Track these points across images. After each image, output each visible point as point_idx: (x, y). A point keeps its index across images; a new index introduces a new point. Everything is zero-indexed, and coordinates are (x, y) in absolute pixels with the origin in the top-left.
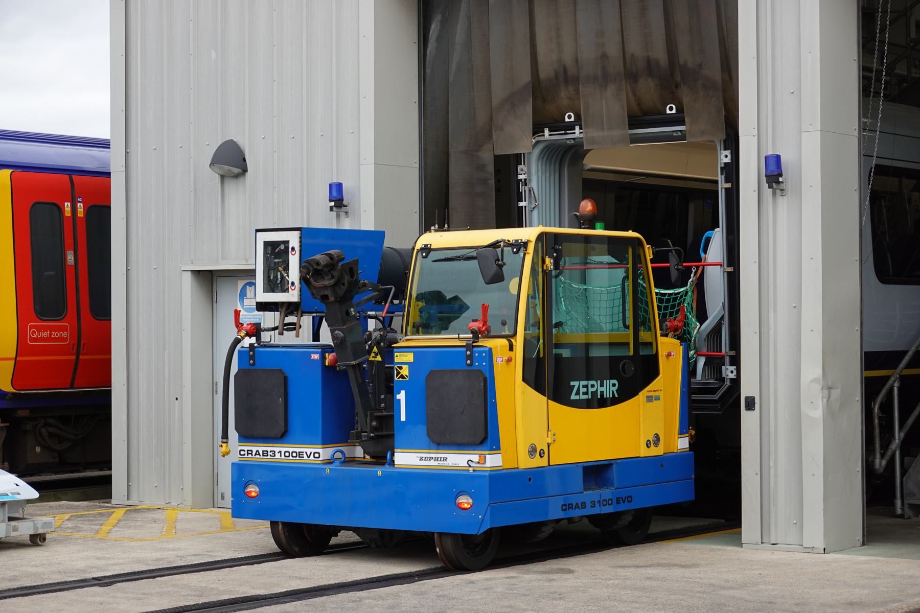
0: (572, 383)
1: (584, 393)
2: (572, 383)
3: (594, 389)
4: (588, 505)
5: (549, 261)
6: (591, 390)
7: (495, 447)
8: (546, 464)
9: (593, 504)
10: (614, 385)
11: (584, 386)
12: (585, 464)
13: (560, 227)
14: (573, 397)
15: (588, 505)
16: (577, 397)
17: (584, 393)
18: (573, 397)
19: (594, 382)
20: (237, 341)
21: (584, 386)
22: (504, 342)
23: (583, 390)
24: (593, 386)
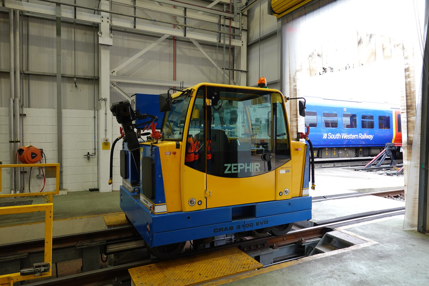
0: (226, 165)
1: (234, 170)
2: (226, 165)
3: (242, 168)
4: (255, 225)
5: (186, 93)
6: (239, 168)
7: (163, 201)
8: (205, 208)
9: (257, 224)
10: (257, 165)
11: (234, 166)
12: (233, 207)
13: (229, 84)
14: (226, 172)
15: (255, 225)
16: (230, 172)
17: (234, 170)
18: (226, 172)
19: (243, 164)
20: (151, 150)
21: (234, 166)
22: (174, 143)
23: (233, 168)
24: (241, 166)
